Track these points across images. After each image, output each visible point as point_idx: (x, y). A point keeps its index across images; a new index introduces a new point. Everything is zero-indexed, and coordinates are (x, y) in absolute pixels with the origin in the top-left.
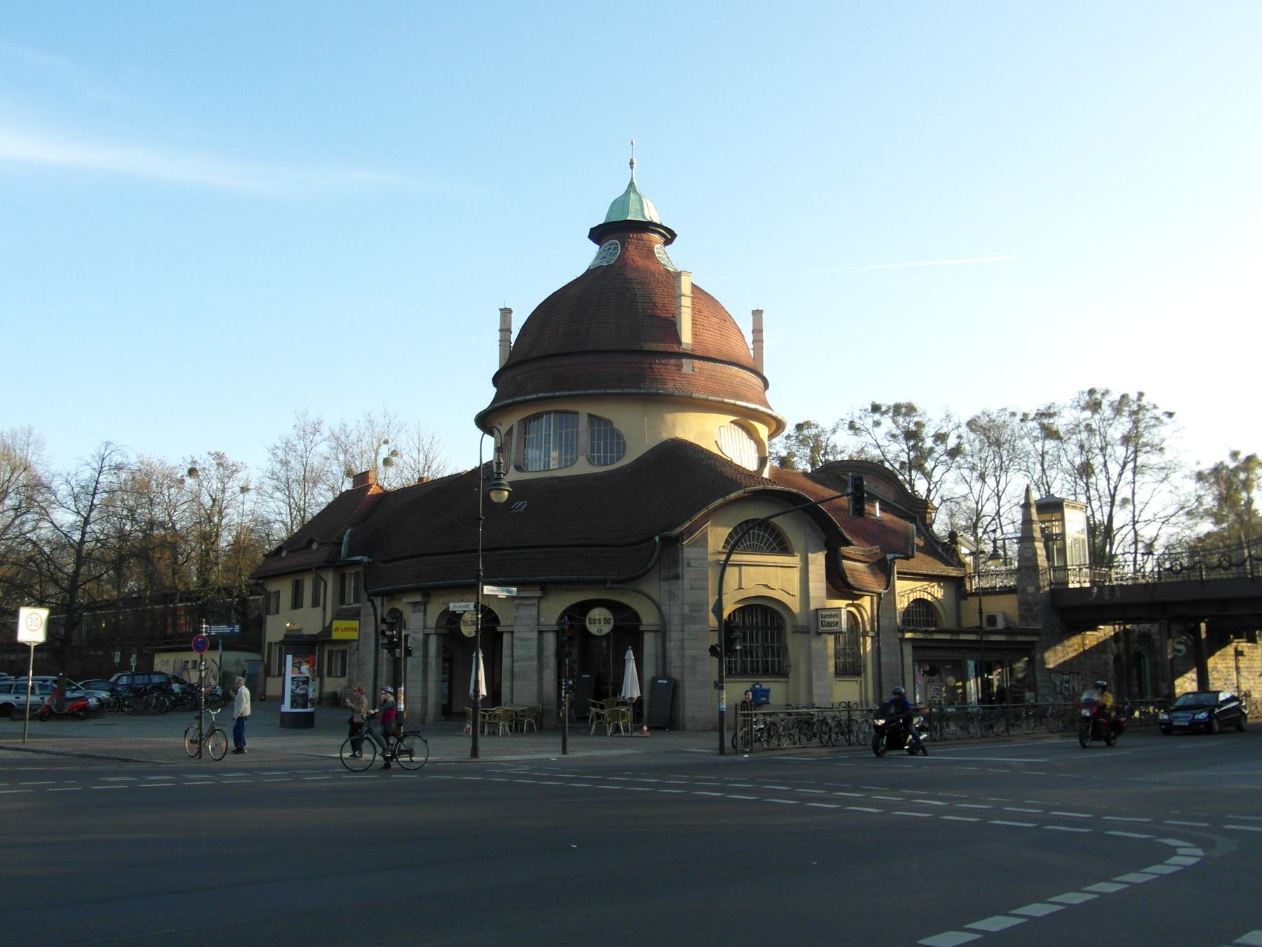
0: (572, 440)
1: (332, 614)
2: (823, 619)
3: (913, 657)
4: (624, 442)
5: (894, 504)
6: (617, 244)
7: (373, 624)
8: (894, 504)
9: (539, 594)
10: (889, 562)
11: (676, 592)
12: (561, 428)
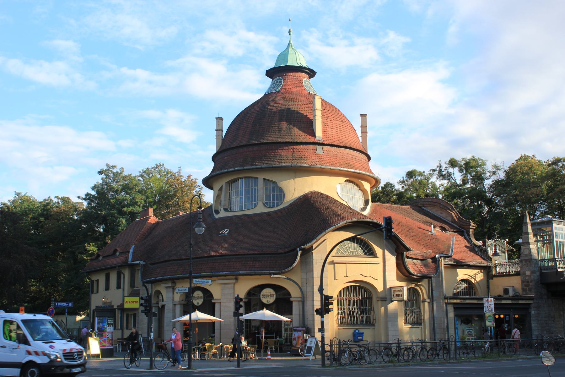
0: (255, 193)
2: (394, 293)
3: (454, 313)
4: (284, 195)
5: (451, 223)
6: (281, 79)
8: (451, 223)
9: (234, 281)
12: (249, 187)
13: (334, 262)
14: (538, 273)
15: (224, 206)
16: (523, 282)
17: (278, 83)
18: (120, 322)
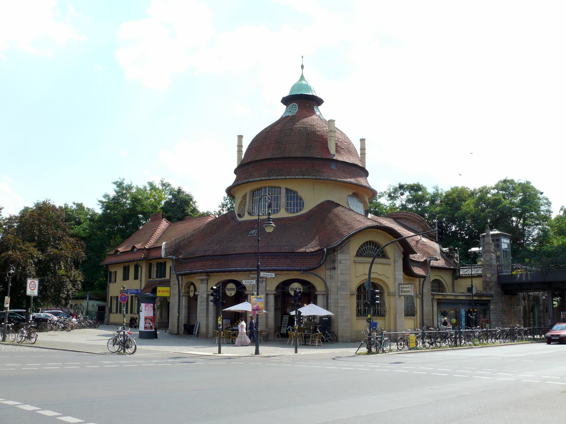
1: (145, 283)
2: (402, 289)
4: (303, 202)
6: (296, 105)
7: (178, 289)
10: (428, 262)
11: (334, 276)
13: (356, 261)
14: (496, 276)
15: (248, 210)
16: (484, 282)
17: (293, 108)
18: (115, 307)
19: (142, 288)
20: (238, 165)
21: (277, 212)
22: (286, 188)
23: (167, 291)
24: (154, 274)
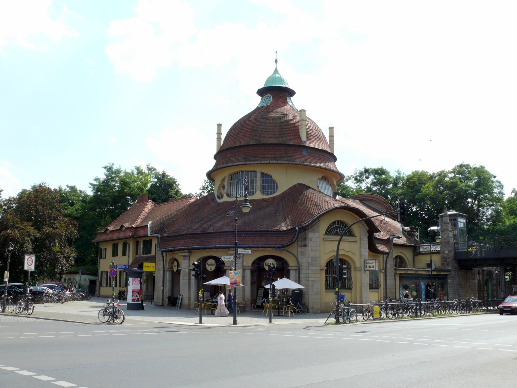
1: (132, 259)
2: (367, 265)
4: (277, 185)
6: (270, 96)
7: (162, 264)
10: (391, 240)
11: (305, 252)
13: (325, 239)
14: (453, 252)
15: (227, 192)
16: (442, 258)
17: (268, 99)
18: (105, 281)
19: (130, 264)
20: (218, 151)
21: (253, 194)
22: (261, 172)
23: (153, 267)
24: (141, 251)
